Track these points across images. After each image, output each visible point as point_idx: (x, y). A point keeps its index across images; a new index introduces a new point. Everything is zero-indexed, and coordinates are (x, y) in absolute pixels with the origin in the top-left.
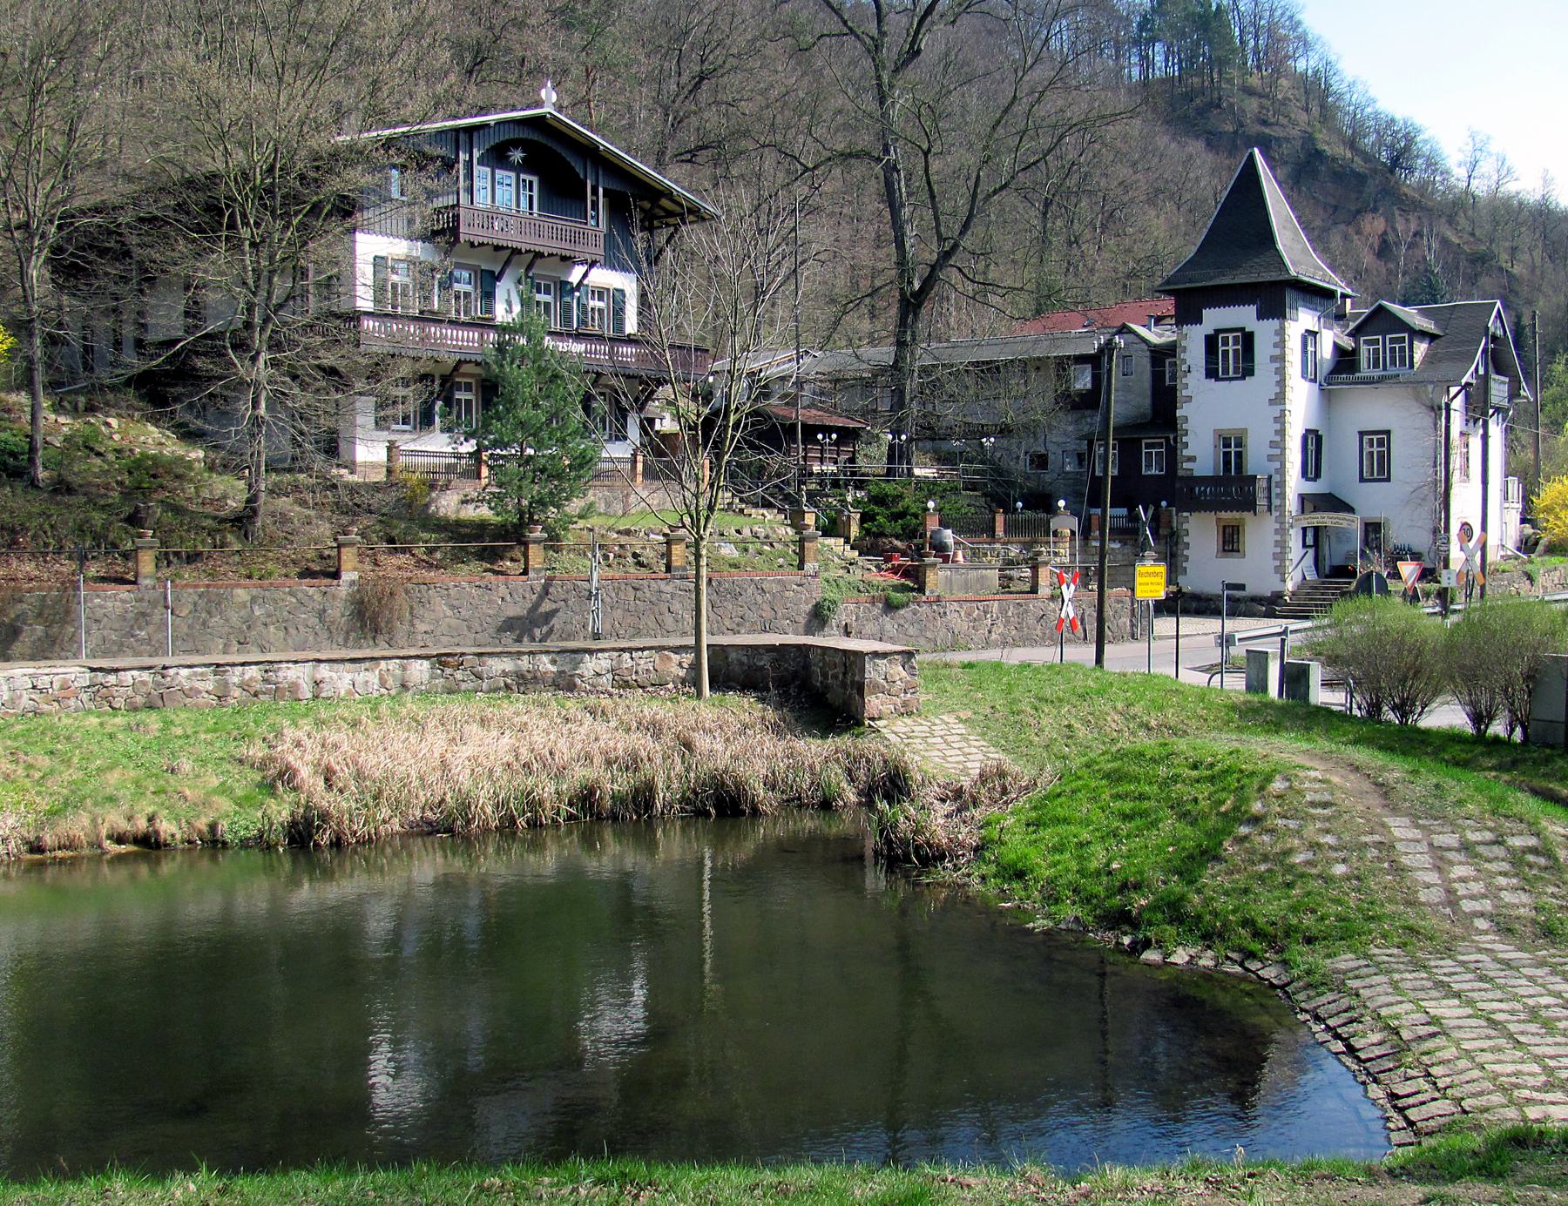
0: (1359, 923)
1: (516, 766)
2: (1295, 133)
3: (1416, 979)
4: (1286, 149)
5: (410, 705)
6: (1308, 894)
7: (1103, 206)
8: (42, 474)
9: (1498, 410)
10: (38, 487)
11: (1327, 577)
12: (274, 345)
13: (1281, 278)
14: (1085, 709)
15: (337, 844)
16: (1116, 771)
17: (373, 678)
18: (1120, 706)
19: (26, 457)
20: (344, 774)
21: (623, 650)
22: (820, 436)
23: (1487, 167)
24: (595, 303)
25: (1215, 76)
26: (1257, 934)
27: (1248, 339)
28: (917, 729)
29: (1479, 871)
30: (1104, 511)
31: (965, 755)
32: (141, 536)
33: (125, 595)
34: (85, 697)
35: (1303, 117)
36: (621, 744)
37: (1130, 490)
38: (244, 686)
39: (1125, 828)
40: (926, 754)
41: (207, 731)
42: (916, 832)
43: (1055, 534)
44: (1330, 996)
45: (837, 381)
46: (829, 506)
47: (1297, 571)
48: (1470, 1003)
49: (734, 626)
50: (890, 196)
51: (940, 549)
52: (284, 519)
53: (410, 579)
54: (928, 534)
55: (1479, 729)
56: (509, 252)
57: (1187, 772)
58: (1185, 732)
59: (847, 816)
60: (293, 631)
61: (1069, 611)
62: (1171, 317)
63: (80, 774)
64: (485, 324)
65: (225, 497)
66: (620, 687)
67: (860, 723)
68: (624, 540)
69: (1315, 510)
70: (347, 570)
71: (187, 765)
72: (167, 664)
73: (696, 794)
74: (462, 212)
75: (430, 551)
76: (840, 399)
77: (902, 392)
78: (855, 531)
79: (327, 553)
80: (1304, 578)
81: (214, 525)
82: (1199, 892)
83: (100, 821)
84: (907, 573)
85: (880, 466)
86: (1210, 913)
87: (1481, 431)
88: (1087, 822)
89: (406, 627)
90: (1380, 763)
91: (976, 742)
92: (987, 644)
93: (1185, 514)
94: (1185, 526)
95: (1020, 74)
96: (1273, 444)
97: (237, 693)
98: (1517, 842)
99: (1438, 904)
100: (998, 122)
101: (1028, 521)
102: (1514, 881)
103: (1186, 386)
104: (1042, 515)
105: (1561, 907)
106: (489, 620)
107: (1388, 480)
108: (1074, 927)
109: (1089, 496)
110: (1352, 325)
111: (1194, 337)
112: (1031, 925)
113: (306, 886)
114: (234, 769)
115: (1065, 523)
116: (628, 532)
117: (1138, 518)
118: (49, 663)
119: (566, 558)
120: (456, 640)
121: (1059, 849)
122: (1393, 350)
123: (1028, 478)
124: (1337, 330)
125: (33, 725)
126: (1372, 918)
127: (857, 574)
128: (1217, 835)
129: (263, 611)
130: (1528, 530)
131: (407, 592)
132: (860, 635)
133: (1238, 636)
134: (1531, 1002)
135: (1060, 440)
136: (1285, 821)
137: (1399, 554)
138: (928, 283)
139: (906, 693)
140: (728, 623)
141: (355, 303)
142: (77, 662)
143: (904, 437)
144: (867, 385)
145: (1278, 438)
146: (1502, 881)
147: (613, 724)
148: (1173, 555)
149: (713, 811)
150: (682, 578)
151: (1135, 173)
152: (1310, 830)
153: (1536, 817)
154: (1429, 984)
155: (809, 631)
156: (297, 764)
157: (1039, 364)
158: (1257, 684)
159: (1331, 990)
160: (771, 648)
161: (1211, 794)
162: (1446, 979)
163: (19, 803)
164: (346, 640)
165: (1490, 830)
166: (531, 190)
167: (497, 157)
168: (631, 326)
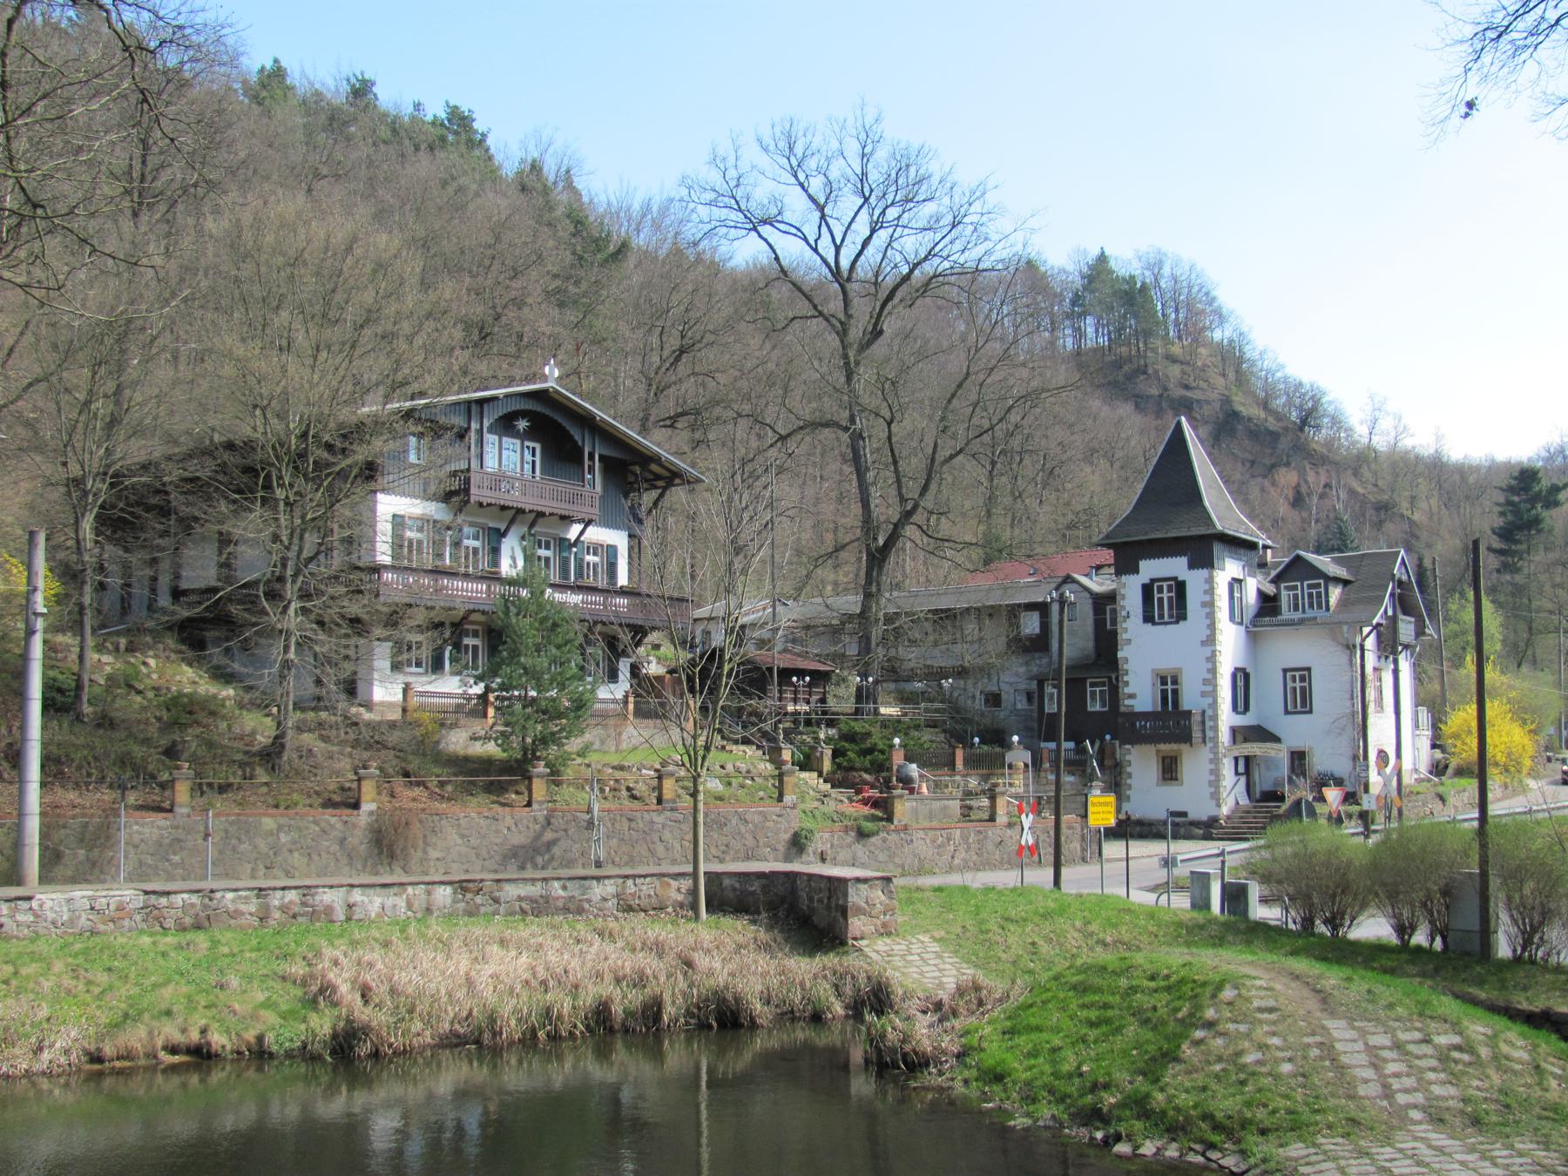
0: (1306, 1116)
2: (1214, 396)
3: (1360, 1165)
4: (1206, 410)
5: (435, 927)
6: (1260, 1090)
7: (1044, 465)
8: (87, 709)
9: (1406, 647)
10: (82, 722)
11: (1258, 801)
12: (305, 595)
13: (1210, 532)
14: (1047, 927)
15: (376, 1055)
16: (1082, 983)
17: (401, 903)
18: (1078, 924)
19: (72, 693)
20: (381, 991)
21: (627, 877)
22: (795, 679)
23: (1385, 424)
24: (590, 558)
26: (1217, 1127)
27: (1180, 587)
28: (896, 947)
29: (1410, 1067)
30: (1059, 746)
31: (940, 970)
32: (178, 768)
33: (162, 823)
34: (138, 918)
35: (1220, 382)
36: (629, 964)
37: (1081, 726)
38: (284, 909)
39: (1093, 1034)
40: (906, 971)
41: (251, 950)
42: (903, 1041)
43: (1010, 767)
45: (808, 628)
46: (803, 742)
47: (1232, 796)
49: (719, 854)
50: (857, 459)
51: (906, 782)
53: (423, 810)
54: (895, 768)
55: (1402, 939)
56: (513, 512)
57: (1146, 983)
58: (1138, 947)
59: (837, 1027)
60: (315, 857)
61: (1028, 839)
62: (1109, 565)
63: (137, 990)
65: (253, 733)
66: (624, 911)
67: (843, 943)
68: (619, 775)
69: (1246, 740)
70: (367, 802)
71: (234, 982)
74: (473, 475)
75: (442, 784)
77: (868, 639)
78: (827, 765)
79: (348, 785)
81: (246, 759)
82: (1162, 1090)
84: (876, 804)
85: (849, 706)
86: (1174, 1109)
87: (1392, 666)
88: (1056, 1030)
89: (420, 854)
90: (1317, 972)
91: (949, 959)
92: (951, 869)
93: (1127, 747)
94: (1128, 757)
95: (972, 352)
96: (1206, 682)
97: (277, 915)
98: (1443, 1040)
101: (987, 755)
102: (1443, 1076)
103: (1126, 630)
104: (998, 749)
105: (1486, 1099)
106: (496, 848)
107: (1310, 712)
108: (1051, 1123)
109: (1042, 729)
110: (1273, 573)
112: (1012, 1123)
114: (278, 985)
115: (1019, 756)
116: (621, 768)
117: (1085, 750)
118: (106, 886)
119: (566, 792)
120: (466, 867)
121: (1033, 1054)
122: (1310, 595)
123: (982, 715)
124: (1260, 577)
125: (91, 944)
126: (1317, 1111)
127: (831, 806)
128: (1177, 1038)
129: (289, 838)
130: (1438, 754)
131: (421, 822)
132: (835, 862)
133: (1180, 858)
135: (1012, 680)
137: (1321, 782)
139: (885, 914)
141: (375, 556)
143: (871, 679)
144: (835, 632)
146: (1431, 1076)
149: (715, 1024)
150: (672, 810)
151: (1072, 434)
155: (788, 859)
157: (992, 612)
158: (1202, 904)
160: (760, 875)
162: (1387, 1164)
164: (364, 866)
166: (534, 455)
167: (505, 425)
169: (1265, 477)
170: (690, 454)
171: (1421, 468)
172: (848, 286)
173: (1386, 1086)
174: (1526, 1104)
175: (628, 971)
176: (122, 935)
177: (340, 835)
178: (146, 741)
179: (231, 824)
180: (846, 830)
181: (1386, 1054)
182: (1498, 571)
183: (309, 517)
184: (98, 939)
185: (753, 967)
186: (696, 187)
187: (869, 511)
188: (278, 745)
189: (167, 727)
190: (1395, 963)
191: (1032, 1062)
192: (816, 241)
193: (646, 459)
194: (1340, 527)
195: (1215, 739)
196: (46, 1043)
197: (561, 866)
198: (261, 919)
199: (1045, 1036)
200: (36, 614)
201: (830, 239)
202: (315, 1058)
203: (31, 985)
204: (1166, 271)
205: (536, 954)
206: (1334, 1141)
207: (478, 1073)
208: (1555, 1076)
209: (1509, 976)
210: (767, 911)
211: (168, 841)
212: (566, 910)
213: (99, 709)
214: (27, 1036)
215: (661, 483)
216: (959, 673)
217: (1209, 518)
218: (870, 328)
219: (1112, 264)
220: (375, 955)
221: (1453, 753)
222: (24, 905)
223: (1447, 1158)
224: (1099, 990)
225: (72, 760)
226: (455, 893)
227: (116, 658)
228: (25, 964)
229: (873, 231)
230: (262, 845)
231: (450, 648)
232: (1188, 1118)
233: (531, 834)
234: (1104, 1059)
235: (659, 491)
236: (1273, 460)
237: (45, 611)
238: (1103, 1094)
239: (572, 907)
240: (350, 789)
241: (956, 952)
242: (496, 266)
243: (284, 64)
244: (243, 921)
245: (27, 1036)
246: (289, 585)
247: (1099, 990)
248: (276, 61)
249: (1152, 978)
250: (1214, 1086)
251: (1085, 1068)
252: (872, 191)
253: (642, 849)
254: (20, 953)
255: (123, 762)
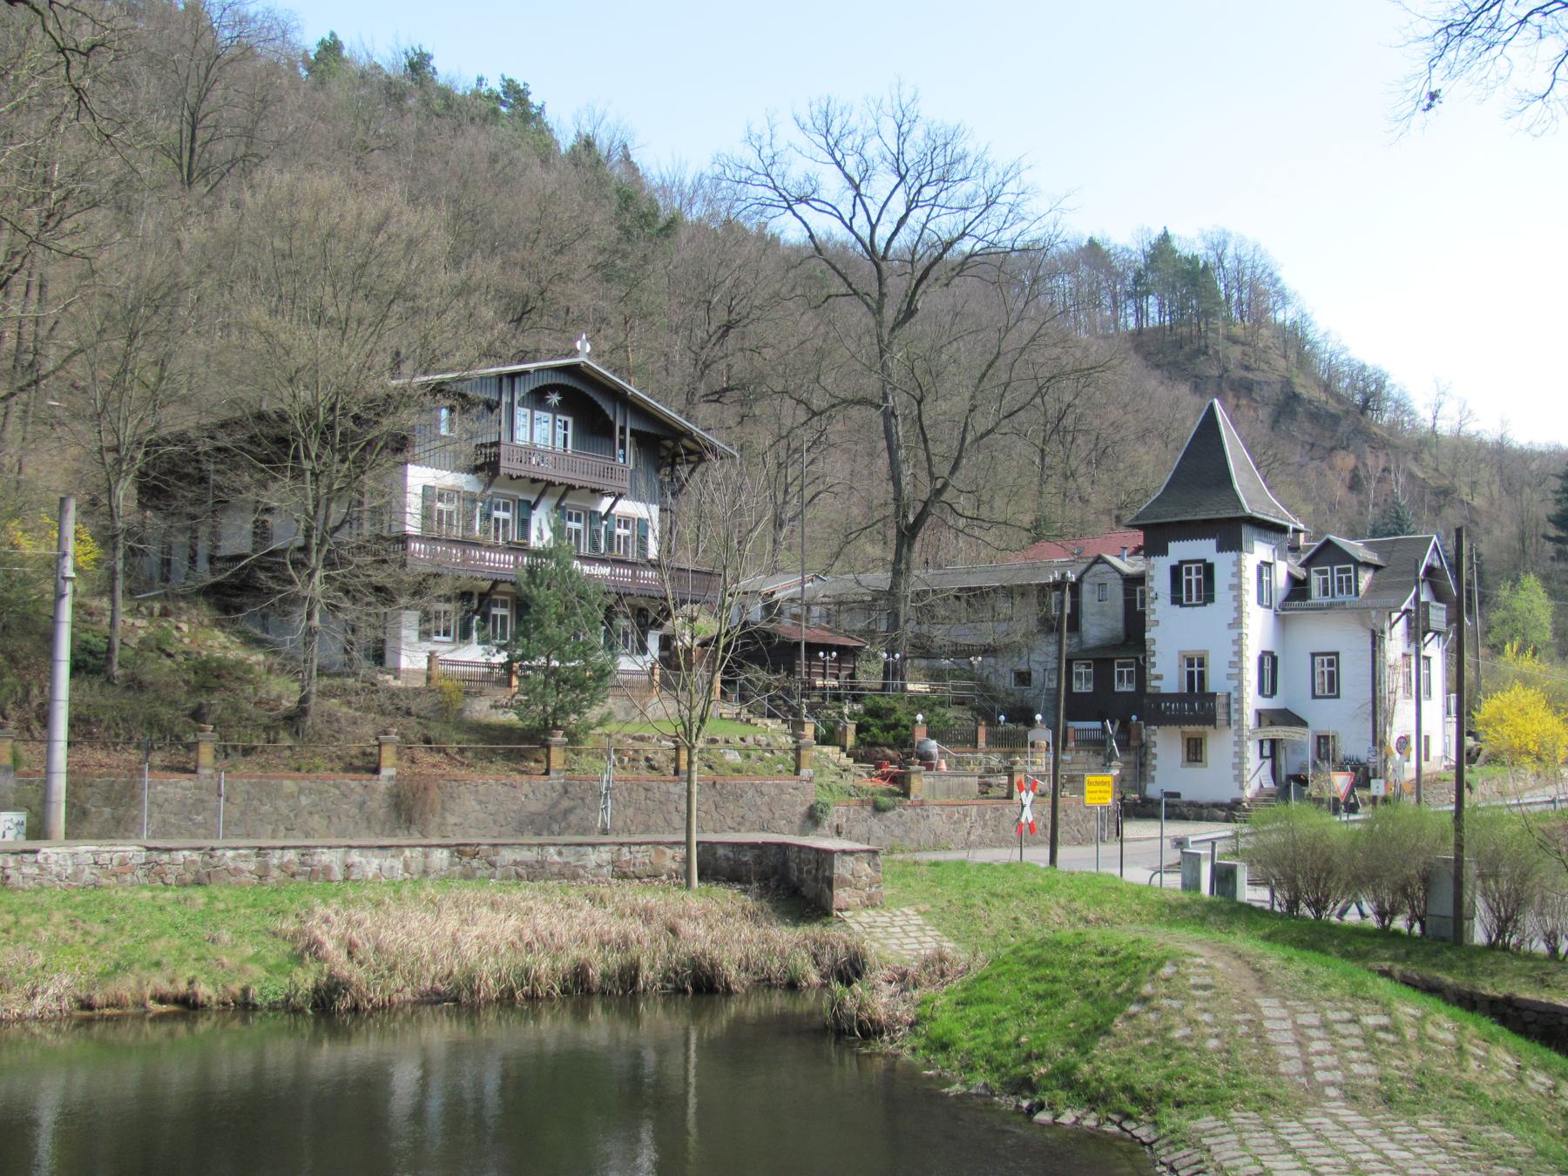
1: (520, 945)
2: (1274, 377)
4: (1267, 392)
6: (1183, 1064)
8: (117, 671)
9: (1437, 633)
10: (113, 684)
12: (329, 564)
13: (1238, 515)
14: (1031, 903)
15: (355, 1009)
16: (1036, 957)
18: (1062, 901)
19: (104, 656)
20: (366, 949)
21: (622, 844)
24: (620, 531)
25: (1202, 326)
26: (1136, 1099)
27: (1208, 570)
28: (879, 919)
29: (1334, 1046)
31: (920, 943)
32: (202, 730)
33: (186, 783)
35: (1281, 364)
36: (614, 928)
38: (283, 867)
39: (1037, 1006)
40: (885, 942)
41: (247, 907)
43: (1033, 745)
44: (1186, 1151)
45: (840, 603)
47: (1256, 776)
48: (1302, 1158)
49: (735, 825)
51: (926, 759)
52: (331, 718)
53: (443, 775)
55: (1383, 922)
56: (543, 484)
60: (335, 820)
61: (1028, 815)
63: (131, 942)
64: (520, 548)
65: (280, 697)
67: (828, 913)
68: (638, 745)
69: (1272, 724)
71: (226, 936)
72: (215, 845)
73: (676, 973)
76: (845, 620)
77: (897, 615)
78: (851, 740)
80: (1262, 786)
82: (1089, 1062)
83: (145, 983)
84: (894, 779)
85: (877, 682)
86: (1097, 1080)
92: (968, 845)
93: (1153, 727)
96: (1232, 664)
97: (276, 873)
98: (1370, 1020)
99: (1294, 1075)
100: (984, 375)
102: (1365, 1055)
103: (1154, 611)
104: (1022, 727)
105: (1402, 1078)
107: (1338, 696)
108: (983, 1091)
110: (1304, 557)
111: (1159, 572)
112: (946, 1090)
113: (326, 1045)
114: (268, 941)
115: (1041, 735)
116: (642, 739)
118: (111, 841)
119: (585, 761)
121: (979, 1025)
122: (1340, 580)
124: (1291, 561)
125: (93, 896)
126: (1235, 1086)
127: (849, 780)
129: (309, 801)
131: (439, 788)
134: (1354, 1157)
135: (1042, 659)
136: (1169, 1001)
138: (921, 519)
139: (870, 887)
140: (729, 821)
142: (138, 842)
143: (897, 656)
144: (868, 607)
145: (1236, 659)
146: (1354, 1055)
147: (609, 910)
148: (1142, 765)
149: (690, 989)
152: (1190, 1009)
153: (1390, 999)
154: (1271, 1142)
156: (325, 938)
157: (1023, 591)
158: (1192, 884)
159: (1188, 1146)
160: (753, 846)
161: (1112, 978)
162: (1287, 1138)
163: (74, 965)
164: (383, 831)
165: (1348, 1010)
166: (566, 429)
167: (538, 398)
168: (653, 551)
169: (1322, 459)
170: (737, 429)
171: (1483, 453)
172: (883, 265)
173: (1307, 1064)
174: (1439, 1084)
175: (614, 935)
176: (124, 889)
177: (360, 799)
178: (173, 703)
179: (252, 785)
180: (862, 804)
181: (1313, 1033)
182: (1552, 559)
183: (335, 487)
184: (100, 893)
185: (736, 936)
186: (731, 165)
187: (900, 489)
188: (302, 710)
189: (194, 690)
190: (1370, 947)
191: (978, 1032)
192: (851, 219)
193: (679, 434)
194: (1397, 512)
195: (1240, 722)
196: (40, 990)
197: (577, 833)
198: (260, 877)
199: (994, 1007)
200: (66, 579)
201: (865, 218)
202: (297, 1011)
203: (30, 934)
204: (1230, 251)
205: (525, 918)
206: (1245, 1115)
207: (461, 1030)
208: (1476, 1058)
209: (1478, 962)
210: (759, 881)
211: (191, 801)
212: (561, 875)
213: (129, 671)
214: (23, 982)
215: (693, 458)
216: (986, 651)
217: (1239, 502)
218: (905, 307)
219: (1175, 244)
220: (366, 915)
221: (1485, 741)
222: (29, 858)
223: (1350, 1134)
224: (1051, 964)
225: (101, 721)
226: (452, 856)
227: (151, 623)
228: (26, 914)
229: (909, 210)
230: (281, 804)
231: (478, 617)
232: (1109, 1090)
233: (549, 802)
234: (1041, 1031)
235: (691, 466)
236: (1333, 443)
237: (73, 575)
238: (1035, 1065)
239: (567, 873)
240: (371, 754)
241: (938, 926)
242: (542, 242)
243: (340, 38)
244: (243, 879)
245: (23, 982)
246: (314, 554)
247: (1051, 964)
248: (333, 35)
249: (1102, 954)
250: (1139, 1059)
251: (1023, 1039)
252: (908, 170)
253: (657, 819)
254: (23, 904)
255: (150, 724)
